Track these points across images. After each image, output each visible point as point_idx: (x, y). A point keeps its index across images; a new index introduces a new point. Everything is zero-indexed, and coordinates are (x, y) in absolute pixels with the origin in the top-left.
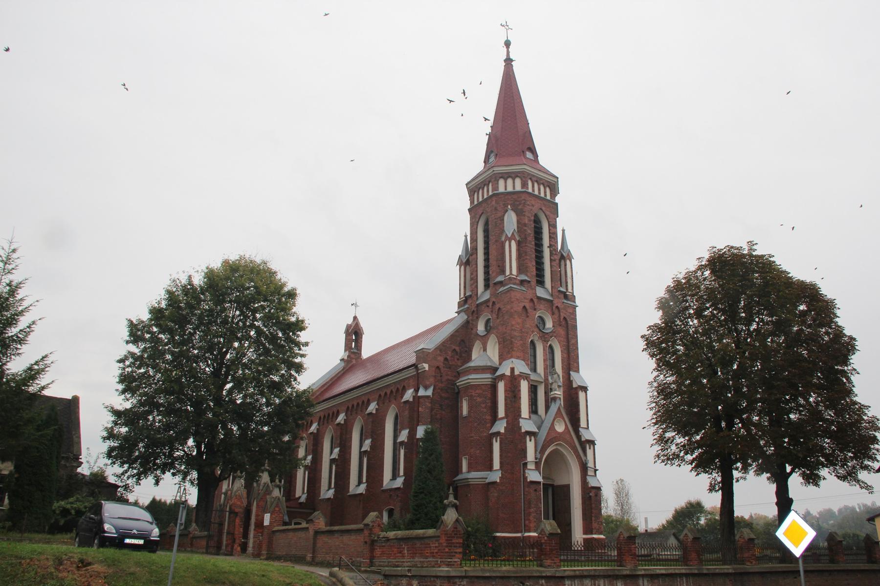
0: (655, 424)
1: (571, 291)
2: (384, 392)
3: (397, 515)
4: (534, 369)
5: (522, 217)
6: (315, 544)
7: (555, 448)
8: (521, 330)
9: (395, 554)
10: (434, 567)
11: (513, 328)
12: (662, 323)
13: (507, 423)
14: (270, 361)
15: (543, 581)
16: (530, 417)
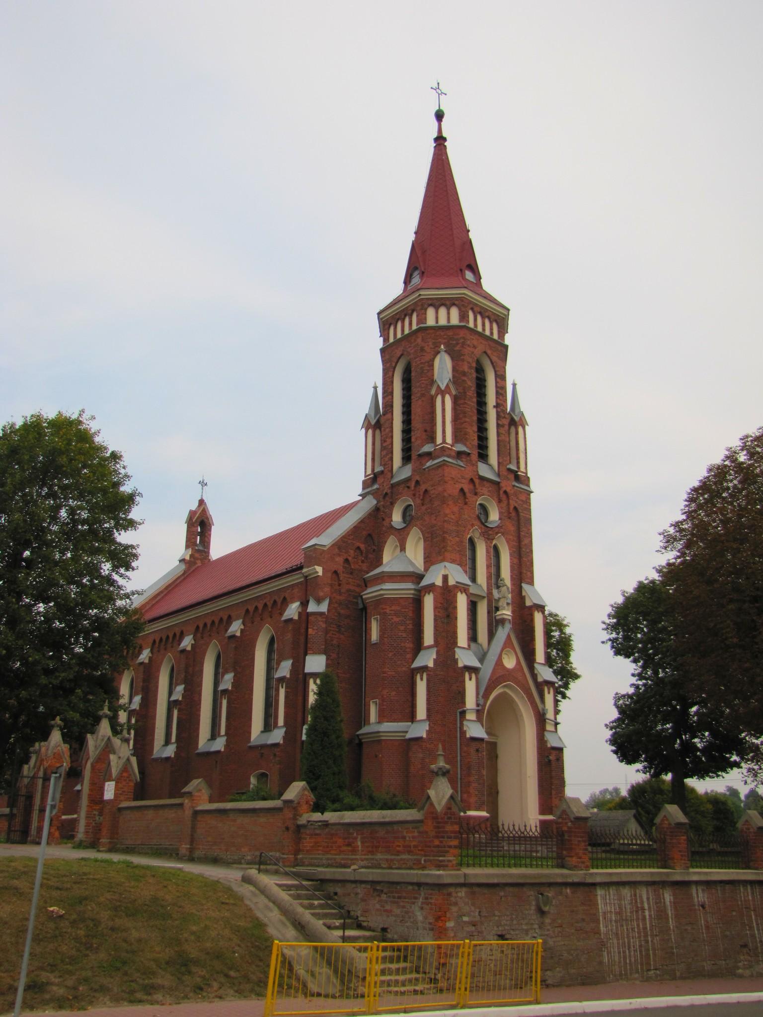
1: (524, 471)
2: (254, 606)
4: (473, 579)
6: (193, 828)
7: (501, 690)
8: (457, 522)
11: (446, 519)
13: (437, 654)
15: (568, 891)
16: (469, 646)
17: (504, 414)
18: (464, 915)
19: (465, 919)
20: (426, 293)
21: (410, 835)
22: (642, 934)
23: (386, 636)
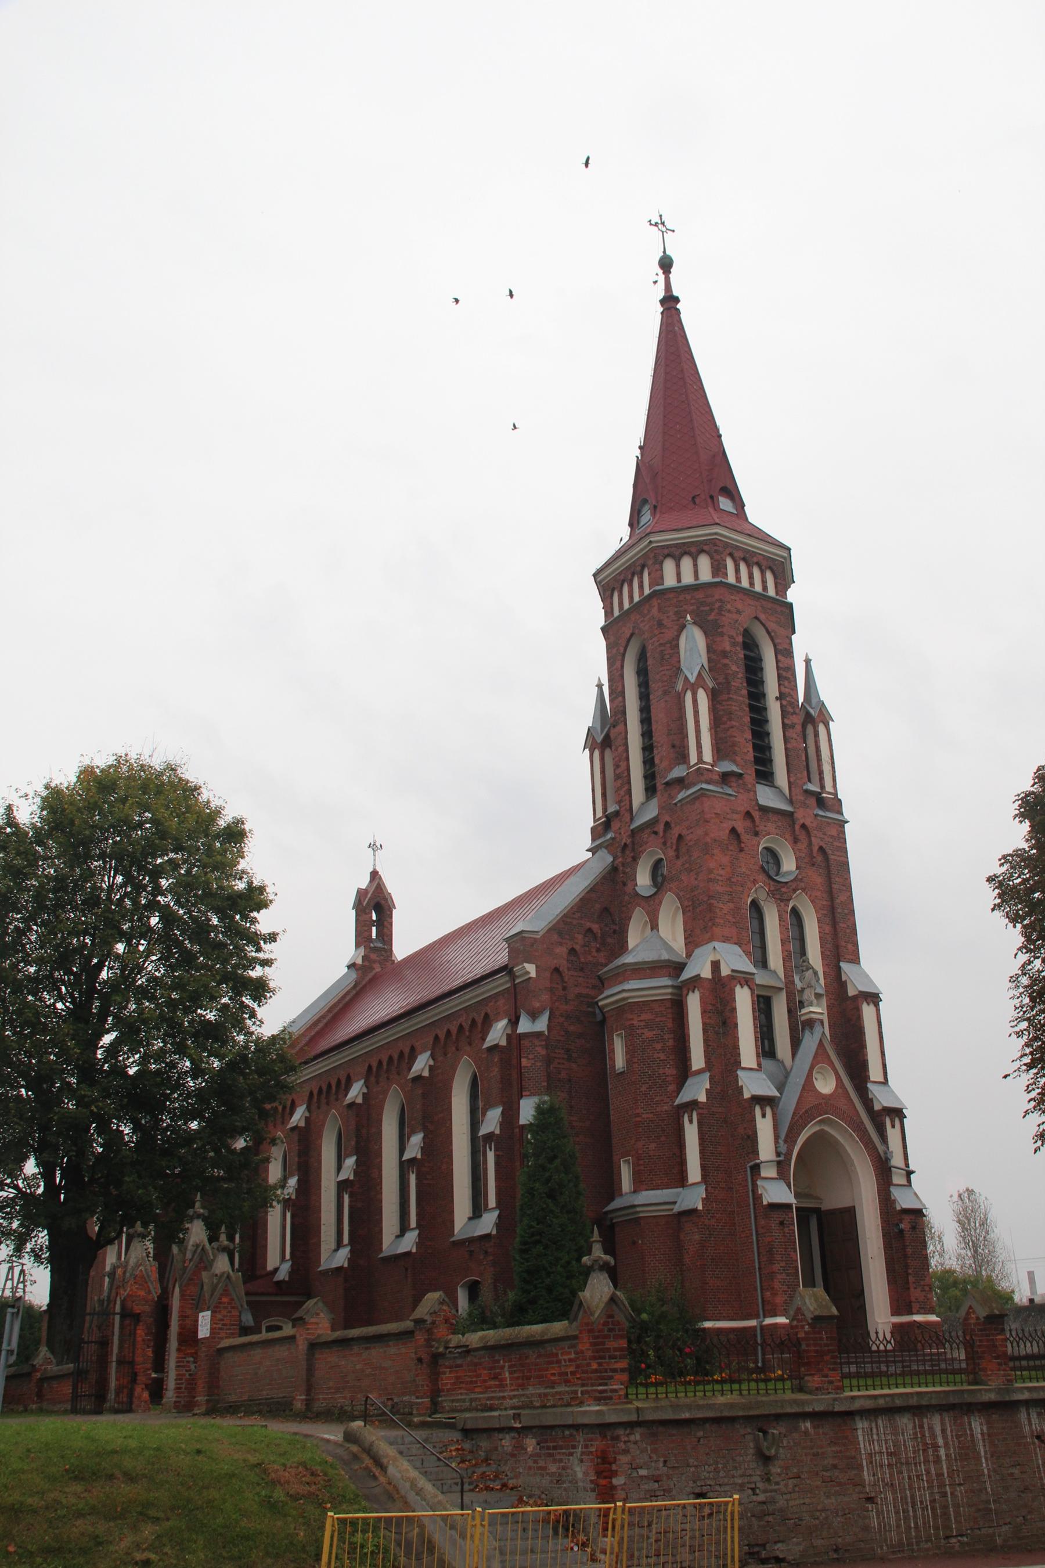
0: (1030, 1066)
1: (832, 791)
2: (445, 1030)
3: (486, 1294)
4: (762, 962)
5: (718, 639)
6: (310, 1370)
7: (817, 1128)
9: (485, 1381)
10: (568, 1405)
11: (712, 876)
12: (1032, 848)
15: (808, 1425)
16: (759, 1065)
17: (793, 708)
18: (641, 1468)
19: (643, 1472)
20: (661, 539)
21: (566, 1357)
23: (635, 1060)
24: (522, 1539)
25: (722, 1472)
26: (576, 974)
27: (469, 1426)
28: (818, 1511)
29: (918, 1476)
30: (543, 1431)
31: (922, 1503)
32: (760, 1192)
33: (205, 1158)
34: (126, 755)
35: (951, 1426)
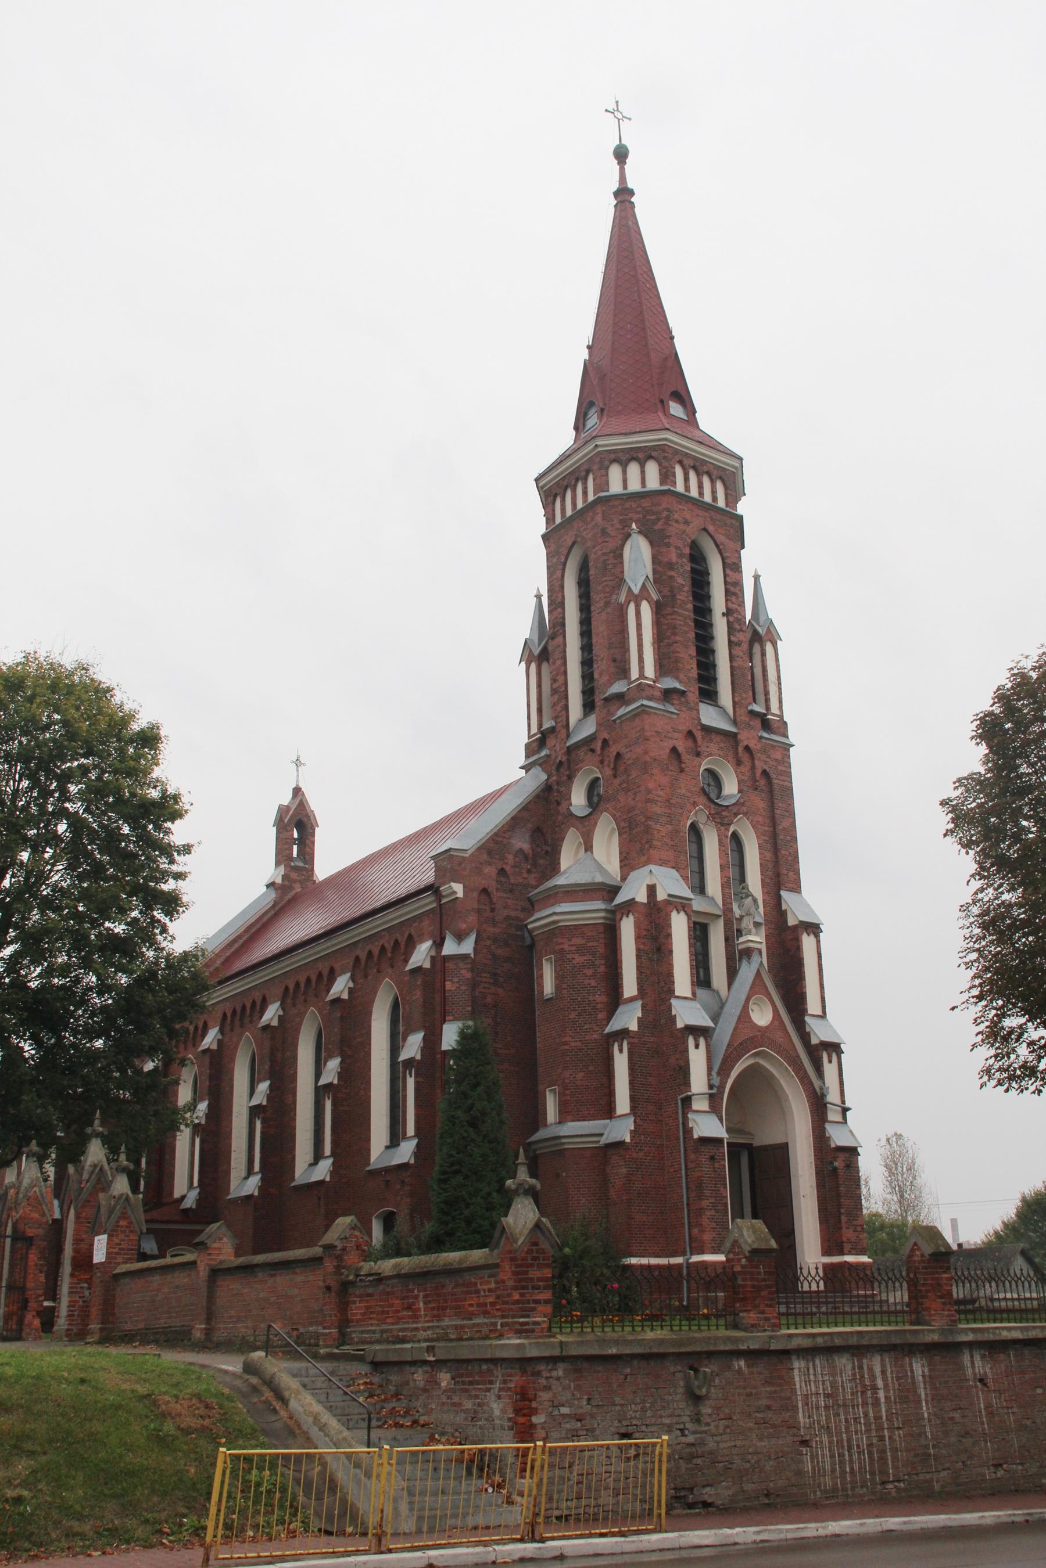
0: (980, 998)
1: (777, 712)
3: (402, 1224)
4: (700, 888)
5: (664, 550)
6: (211, 1297)
7: (751, 1061)
8: (668, 801)
9: (397, 1311)
10: (486, 1338)
12: (989, 770)
14: (104, 890)
15: (742, 1363)
16: (694, 994)
17: (740, 625)
18: (563, 1406)
19: (565, 1410)
21: (486, 1287)
22: (873, 1426)
24: (432, 1478)
25: (649, 1411)
26: (505, 895)
27: (378, 1359)
28: (750, 1454)
29: (855, 1419)
30: (457, 1364)
31: (858, 1446)
32: (690, 1126)
33: (111, 1078)
34: (35, 652)
35: (891, 1368)
